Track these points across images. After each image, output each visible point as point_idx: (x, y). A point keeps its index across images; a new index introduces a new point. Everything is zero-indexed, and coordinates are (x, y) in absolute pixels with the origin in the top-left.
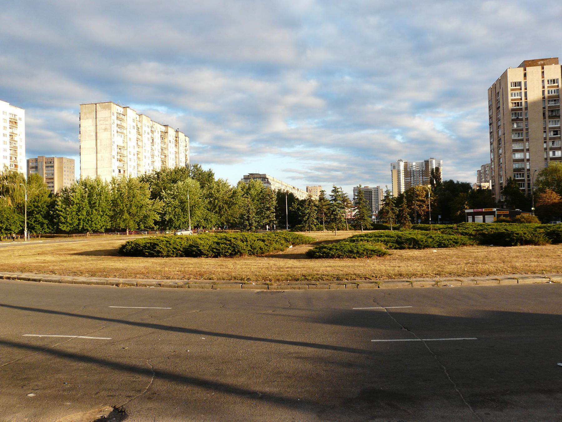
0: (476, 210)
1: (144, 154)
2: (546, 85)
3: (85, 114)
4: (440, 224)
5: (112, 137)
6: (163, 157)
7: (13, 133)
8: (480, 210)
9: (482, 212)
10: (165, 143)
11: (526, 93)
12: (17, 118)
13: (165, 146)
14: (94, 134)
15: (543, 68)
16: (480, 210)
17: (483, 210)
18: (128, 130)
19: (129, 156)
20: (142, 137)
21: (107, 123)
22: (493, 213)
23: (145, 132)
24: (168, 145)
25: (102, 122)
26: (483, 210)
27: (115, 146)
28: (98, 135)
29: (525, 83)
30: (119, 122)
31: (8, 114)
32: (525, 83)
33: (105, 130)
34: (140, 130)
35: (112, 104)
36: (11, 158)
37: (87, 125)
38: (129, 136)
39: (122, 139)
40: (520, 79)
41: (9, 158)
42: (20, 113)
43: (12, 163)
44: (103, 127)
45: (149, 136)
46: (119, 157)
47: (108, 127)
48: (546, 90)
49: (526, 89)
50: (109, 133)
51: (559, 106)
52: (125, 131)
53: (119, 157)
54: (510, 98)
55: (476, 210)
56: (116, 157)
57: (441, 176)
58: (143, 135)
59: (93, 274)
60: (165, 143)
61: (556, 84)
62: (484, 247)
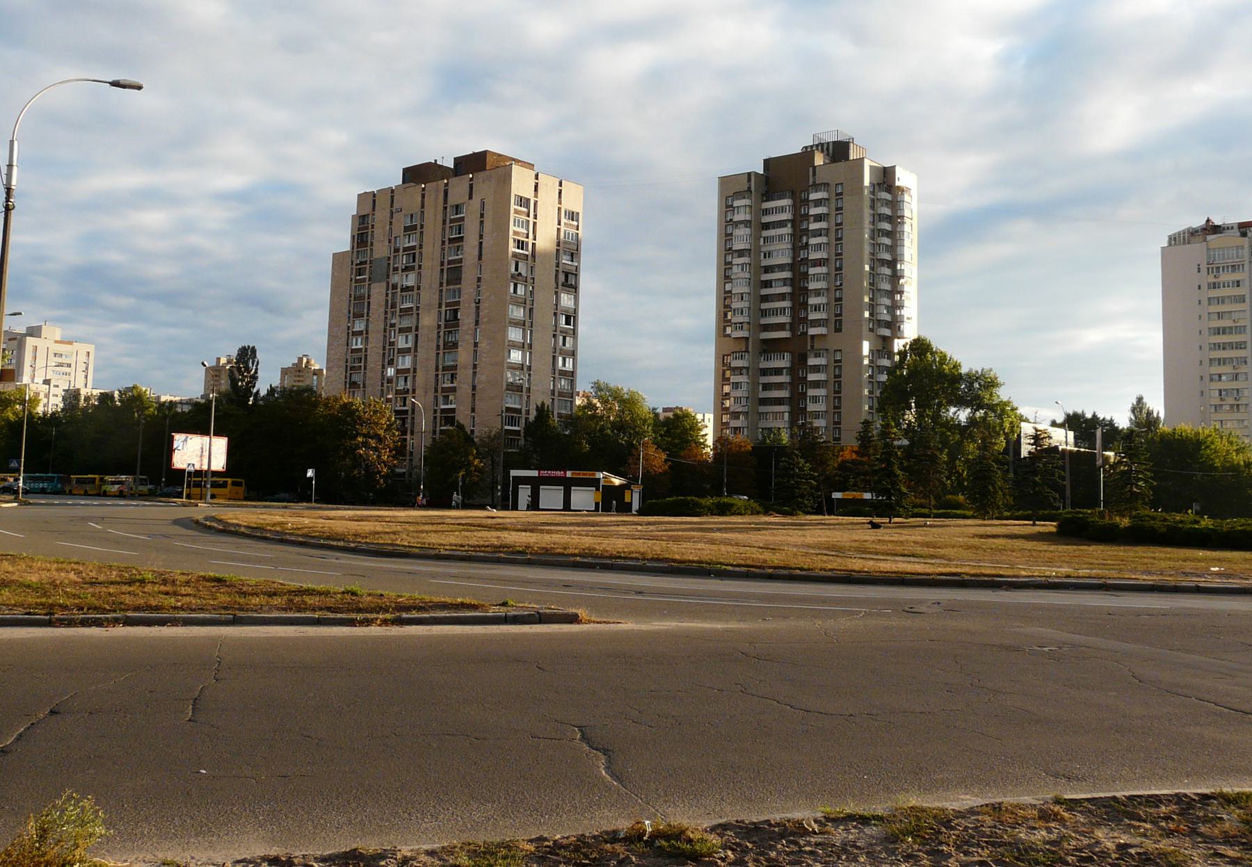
0: (545, 473)
2: (563, 221)
4: (465, 506)
8: (559, 473)
9: (565, 478)
11: (535, 224)
15: (560, 184)
16: (559, 473)
17: (569, 474)
22: (594, 483)
26: (569, 474)
29: (536, 203)
32: (536, 203)
40: (528, 193)
48: (563, 228)
49: (535, 217)
51: (460, 261)
54: (512, 228)
55: (545, 473)
57: (657, 397)
61: (575, 223)
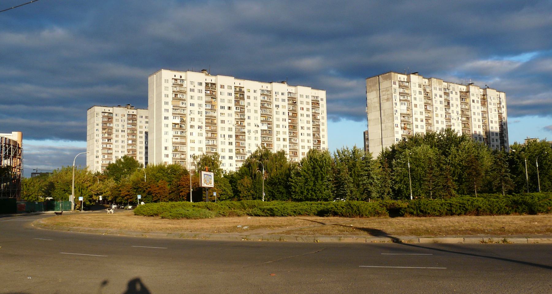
1: (436, 119)
3: (370, 87)
5: (394, 105)
6: (464, 119)
7: (315, 113)
10: (466, 104)
12: (319, 99)
13: (467, 107)
14: (378, 105)
18: (413, 96)
19: (415, 123)
20: (432, 101)
21: (389, 93)
23: (436, 95)
24: (470, 105)
25: (384, 93)
27: (398, 115)
28: (382, 106)
30: (402, 90)
31: (310, 97)
33: (388, 100)
34: (429, 95)
35: (393, 74)
36: (314, 135)
37: (372, 97)
38: (414, 102)
39: (406, 106)
41: (312, 135)
42: (322, 94)
43: (315, 139)
44: (386, 97)
45: (442, 99)
46: (403, 126)
47: (390, 96)
50: (390, 102)
52: (409, 98)
53: (403, 126)
56: (399, 126)
58: (434, 100)
59: (494, 233)
60: (466, 104)
62: (515, 242)
